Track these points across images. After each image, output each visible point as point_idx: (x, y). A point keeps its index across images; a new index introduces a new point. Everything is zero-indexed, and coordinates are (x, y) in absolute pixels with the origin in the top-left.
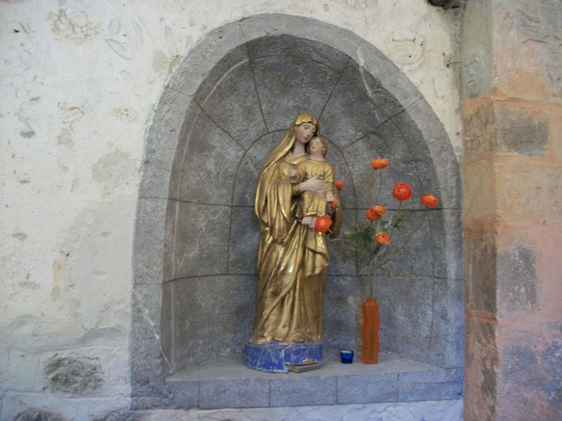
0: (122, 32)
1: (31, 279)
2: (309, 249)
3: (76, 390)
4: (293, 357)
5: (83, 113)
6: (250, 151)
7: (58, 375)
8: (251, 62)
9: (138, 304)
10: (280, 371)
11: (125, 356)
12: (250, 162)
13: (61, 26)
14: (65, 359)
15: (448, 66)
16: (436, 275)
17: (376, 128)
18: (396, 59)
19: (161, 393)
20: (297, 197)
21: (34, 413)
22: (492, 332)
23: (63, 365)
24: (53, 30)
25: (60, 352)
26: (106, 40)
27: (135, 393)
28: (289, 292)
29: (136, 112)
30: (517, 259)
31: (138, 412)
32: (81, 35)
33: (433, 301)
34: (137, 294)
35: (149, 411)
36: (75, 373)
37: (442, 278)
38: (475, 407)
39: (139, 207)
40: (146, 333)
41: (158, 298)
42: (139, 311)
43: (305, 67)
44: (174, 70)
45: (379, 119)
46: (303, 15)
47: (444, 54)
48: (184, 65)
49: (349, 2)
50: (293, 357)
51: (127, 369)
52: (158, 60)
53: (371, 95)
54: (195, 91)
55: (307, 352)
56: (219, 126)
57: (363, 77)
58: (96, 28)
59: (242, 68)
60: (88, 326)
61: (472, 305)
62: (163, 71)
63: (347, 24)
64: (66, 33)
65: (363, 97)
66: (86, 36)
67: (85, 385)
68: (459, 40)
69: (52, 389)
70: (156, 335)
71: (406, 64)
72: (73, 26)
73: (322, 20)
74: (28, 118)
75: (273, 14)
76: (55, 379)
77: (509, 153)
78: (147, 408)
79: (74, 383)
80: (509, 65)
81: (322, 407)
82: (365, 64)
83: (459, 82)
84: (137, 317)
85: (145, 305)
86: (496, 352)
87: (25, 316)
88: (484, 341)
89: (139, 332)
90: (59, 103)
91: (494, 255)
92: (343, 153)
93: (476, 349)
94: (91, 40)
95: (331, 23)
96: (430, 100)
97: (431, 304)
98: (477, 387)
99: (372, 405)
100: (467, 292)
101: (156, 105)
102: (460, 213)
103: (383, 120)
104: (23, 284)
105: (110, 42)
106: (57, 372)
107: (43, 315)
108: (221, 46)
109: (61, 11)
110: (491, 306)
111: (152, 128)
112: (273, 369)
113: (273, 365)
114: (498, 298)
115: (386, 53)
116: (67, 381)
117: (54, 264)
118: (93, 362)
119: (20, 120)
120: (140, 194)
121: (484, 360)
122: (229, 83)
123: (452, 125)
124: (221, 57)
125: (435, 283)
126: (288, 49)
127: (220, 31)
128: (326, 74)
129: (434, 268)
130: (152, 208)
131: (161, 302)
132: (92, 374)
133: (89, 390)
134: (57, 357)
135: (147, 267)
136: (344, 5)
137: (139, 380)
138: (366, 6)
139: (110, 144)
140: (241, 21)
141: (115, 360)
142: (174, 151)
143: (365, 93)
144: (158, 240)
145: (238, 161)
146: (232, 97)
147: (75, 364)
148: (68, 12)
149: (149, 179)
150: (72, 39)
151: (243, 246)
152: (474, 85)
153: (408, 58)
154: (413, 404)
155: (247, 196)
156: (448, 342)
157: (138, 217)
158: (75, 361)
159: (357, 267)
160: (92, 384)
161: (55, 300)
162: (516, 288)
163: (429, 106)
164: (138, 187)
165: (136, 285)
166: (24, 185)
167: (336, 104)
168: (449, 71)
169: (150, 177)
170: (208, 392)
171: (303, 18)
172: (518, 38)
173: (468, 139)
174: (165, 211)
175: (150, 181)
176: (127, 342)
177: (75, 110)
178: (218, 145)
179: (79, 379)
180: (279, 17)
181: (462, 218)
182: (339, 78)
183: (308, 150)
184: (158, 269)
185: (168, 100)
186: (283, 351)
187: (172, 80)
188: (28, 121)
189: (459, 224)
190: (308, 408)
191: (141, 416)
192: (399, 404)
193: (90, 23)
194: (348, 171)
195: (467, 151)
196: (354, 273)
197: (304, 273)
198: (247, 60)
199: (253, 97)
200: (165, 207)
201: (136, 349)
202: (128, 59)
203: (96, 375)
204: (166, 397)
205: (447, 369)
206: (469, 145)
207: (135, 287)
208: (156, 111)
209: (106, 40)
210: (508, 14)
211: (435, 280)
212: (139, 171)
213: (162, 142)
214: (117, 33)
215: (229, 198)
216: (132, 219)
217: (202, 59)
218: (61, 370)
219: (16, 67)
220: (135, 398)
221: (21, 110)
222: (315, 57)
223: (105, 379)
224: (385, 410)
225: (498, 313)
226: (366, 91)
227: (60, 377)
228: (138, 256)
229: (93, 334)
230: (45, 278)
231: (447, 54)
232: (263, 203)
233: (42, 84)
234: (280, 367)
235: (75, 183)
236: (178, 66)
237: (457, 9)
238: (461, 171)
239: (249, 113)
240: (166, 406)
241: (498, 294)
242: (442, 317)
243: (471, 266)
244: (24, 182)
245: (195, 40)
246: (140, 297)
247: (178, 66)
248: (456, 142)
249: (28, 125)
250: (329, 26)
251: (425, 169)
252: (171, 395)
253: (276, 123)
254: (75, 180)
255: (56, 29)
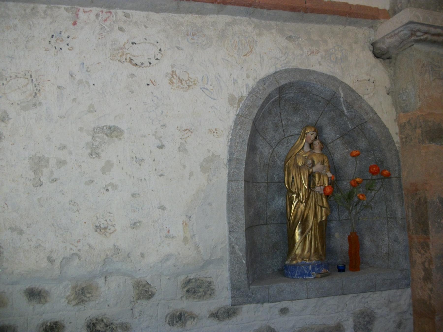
0: (209, 83)
1: (171, 233)
2: (319, 205)
3: (200, 296)
4: (316, 269)
5: (192, 132)
6: (276, 149)
7: (189, 288)
8: (279, 97)
9: (232, 244)
10: (310, 278)
11: (226, 275)
12: (275, 155)
13: (174, 81)
14: (192, 279)
15: (388, 94)
16: (389, 216)
17: (348, 132)
18: (360, 92)
19: (248, 295)
20: (311, 176)
21: (177, 312)
22: (428, 246)
23: (192, 282)
24: (170, 83)
25: (189, 275)
26: (201, 88)
27: (233, 296)
28: (309, 232)
29: (222, 131)
30: (438, 204)
31: (235, 307)
32: (186, 86)
33: (388, 232)
34: (231, 237)
35: (241, 306)
36: (199, 287)
37: (393, 218)
38: (419, 291)
39: (229, 186)
40: (238, 260)
41: (243, 240)
42: (233, 247)
43: (308, 98)
44: (241, 105)
45: (350, 127)
46: (308, 69)
47: (386, 87)
48: (246, 102)
49: (332, 59)
50: (316, 269)
51: (229, 282)
52: (232, 100)
53: (346, 113)
54: (254, 117)
55: (323, 265)
56: (261, 136)
57: (343, 103)
58: (194, 82)
59: (275, 101)
60: (206, 258)
61: (413, 232)
62: (234, 105)
63: (332, 73)
64: (177, 85)
65: (342, 114)
66: (189, 86)
67: (205, 293)
68: (394, 79)
69: (186, 297)
70: (243, 261)
71: (366, 94)
72: (181, 81)
73: (319, 71)
74: (161, 137)
75: (292, 69)
76: (188, 291)
77: (430, 145)
78: (240, 305)
79: (198, 293)
80: (426, 94)
81: (336, 297)
82: (344, 96)
83: (396, 104)
84: (232, 251)
85: (236, 243)
86: (431, 257)
87: (168, 255)
88: (423, 252)
89: (234, 260)
90: (177, 127)
91: (426, 202)
92: (328, 148)
93: (418, 258)
94: (192, 88)
95: (324, 72)
96: (379, 114)
97: (387, 233)
98: (420, 279)
99: (362, 294)
100: (409, 225)
101: (233, 126)
102: (401, 180)
103: (353, 128)
104: (166, 237)
105: (203, 89)
106: (189, 287)
107: (179, 254)
108: (265, 89)
109: (173, 71)
110: (426, 231)
111: (231, 140)
112: (306, 277)
113: (305, 274)
114: (430, 226)
115: (354, 88)
116: (195, 291)
117: (183, 223)
118: (208, 280)
119: (156, 138)
120: (228, 179)
121: (423, 263)
122: (268, 110)
123: (394, 130)
124: (266, 96)
125: (388, 221)
126: (300, 88)
127: (263, 81)
128: (320, 101)
129: (387, 212)
130: (236, 187)
131: (245, 241)
132: (209, 286)
133: (207, 296)
134: (188, 278)
135: (235, 221)
136: (329, 61)
137: (235, 288)
138: (342, 61)
139: (209, 151)
140: (274, 74)
141: (222, 277)
142: (246, 153)
143: (343, 112)
144: (241, 205)
145: (269, 155)
146: (268, 118)
147: (198, 282)
148: (177, 72)
149: (233, 170)
150: (181, 88)
151: (273, 206)
152: (406, 106)
153: (366, 91)
154: (384, 292)
155: (275, 176)
156: (400, 254)
157: (228, 193)
158: (199, 279)
159: (339, 215)
160: (209, 292)
161: (185, 244)
162: (439, 220)
163: (380, 118)
164: (227, 175)
165: (230, 232)
166: (162, 177)
167: (325, 119)
168: (389, 97)
169: (233, 169)
170: (274, 293)
171: (308, 71)
172: (430, 78)
173: (403, 136)
174: (243, 188)
175: (234, 171)
176: (228, 266)
177: (188, 131)
178: (260, 147)
179: (201, 290)
180: (296, 70)
181: (402, 182)
182: (328, 104)
183: (312, 147)
184: (242, 222)
185: (239, 123)
186: (310, 266)
187: (241, 111)
188: (161, 139)
189: (401, 186)
190: (328, 298)
191: (237, 309)
192: (376, 292)
193: (191, 78)
194: (331, 158)
195: (403, 143)
196: (337, 219)
197: (317, 220)
198: (278, 96)
199: (279, 117)
200: (243, 186)
201: (232, 270)
202: (215, 99)
203: (211, 287)
204: (250, 297)
205: (401, 271)
206: (404, 140)
207: (230, 234)
208: (233, 130)
209: (201, 88)
210: (423, 65)
211: (389, 219)
212: (226, 165)
213: (238, 148)
214: (207, 84)
215: (266, 178)
216: (225, 193)
217: (256, 97)
218: (190, 286)
219: (150, 106)
220: (233, 299)
221: (156, 132)
222: (314, 92)
223: (216, 289)
224: (369, 297)
225: (430, 235)
226: (344, 111)
227: (190, 290)
228: (230, 215)
229: (208, 263)
230: (178, 230)
231: (387, 87)
232: (291, 179)
233: (166, 116)
234: (310, 275)
235: (191, 174)
236: (243, 102)
237: (391, 60)
238: (400, 155)
239: (276, 126)
240: (250, 303)
241: (430, 225)
242: (395, 241)
243: (410, 210)
244: (161, 175)
245: (251, 86)
246: (233, 239)
247: (243, 102)
248: (396, 139)
249: (161, 141)
250: (322, 74)
251: (379, 155)
252: (253, 296)
253: (289, 131)
254: (191, 172)
255: (172, 83)
